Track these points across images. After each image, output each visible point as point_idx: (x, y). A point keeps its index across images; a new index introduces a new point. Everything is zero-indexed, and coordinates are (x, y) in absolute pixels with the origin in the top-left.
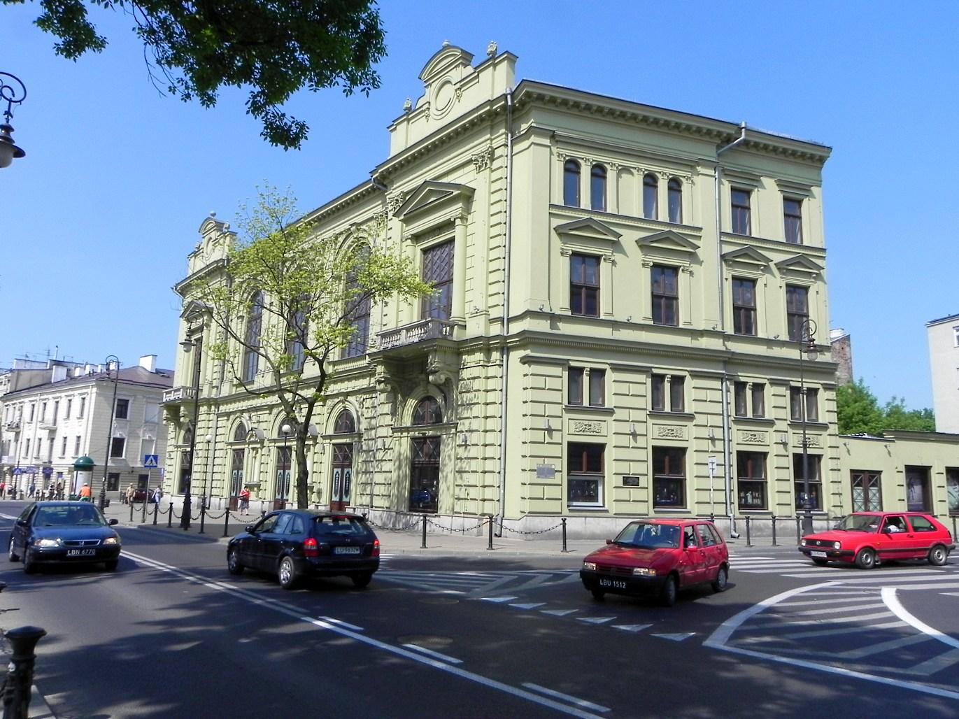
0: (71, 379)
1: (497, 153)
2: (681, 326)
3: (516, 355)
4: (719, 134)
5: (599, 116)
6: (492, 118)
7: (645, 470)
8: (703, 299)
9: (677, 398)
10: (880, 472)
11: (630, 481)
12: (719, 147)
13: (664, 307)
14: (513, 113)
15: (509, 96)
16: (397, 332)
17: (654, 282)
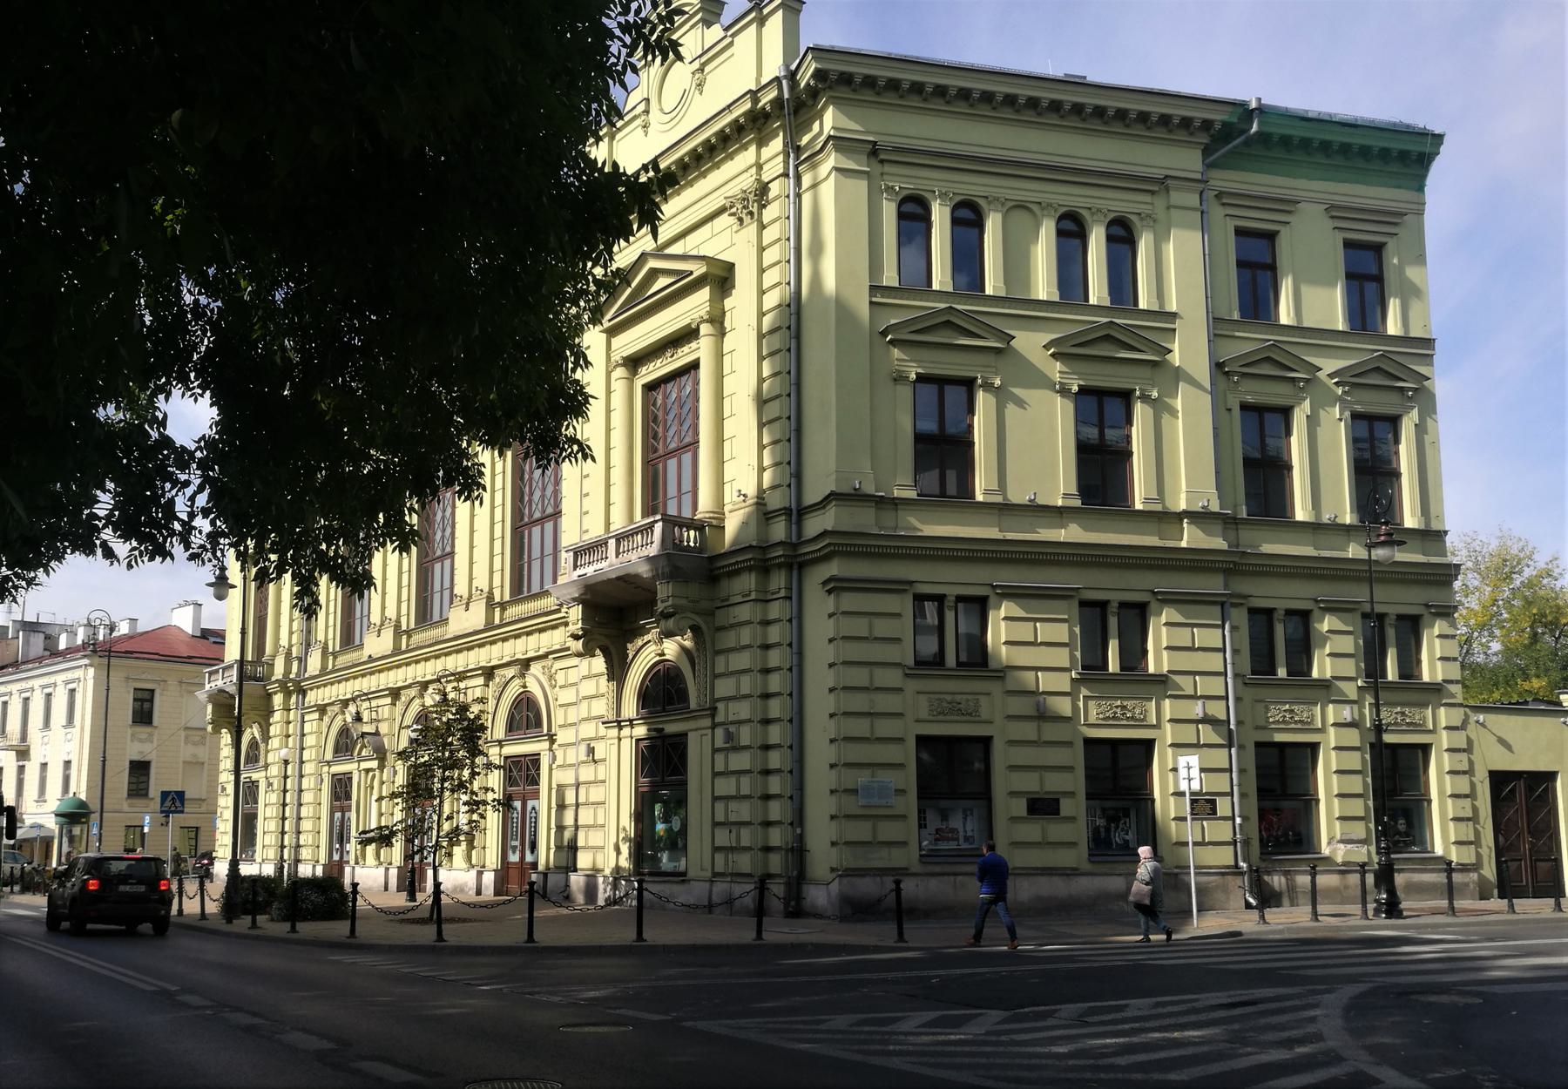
0: (52, 652)
1: (775, 189)
2: (1139, 506)
3: (817, 576)
4: (1207, 125)
5: (1008, 113)
6: (758, 124)
7: (1072, 784)
8: (1179, 458)
9: (1134, 654)
10: (1551, 776)
11: (1043, 807)
12: (1207, 151)
13: (1102, 469)
14: (796, 112)
15: (784, 82)
16: (600, 545)
17: (1080, 419)
